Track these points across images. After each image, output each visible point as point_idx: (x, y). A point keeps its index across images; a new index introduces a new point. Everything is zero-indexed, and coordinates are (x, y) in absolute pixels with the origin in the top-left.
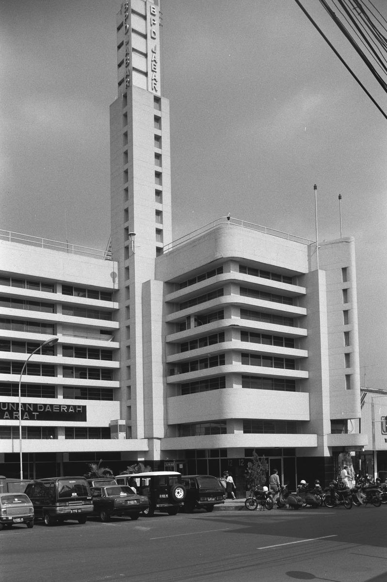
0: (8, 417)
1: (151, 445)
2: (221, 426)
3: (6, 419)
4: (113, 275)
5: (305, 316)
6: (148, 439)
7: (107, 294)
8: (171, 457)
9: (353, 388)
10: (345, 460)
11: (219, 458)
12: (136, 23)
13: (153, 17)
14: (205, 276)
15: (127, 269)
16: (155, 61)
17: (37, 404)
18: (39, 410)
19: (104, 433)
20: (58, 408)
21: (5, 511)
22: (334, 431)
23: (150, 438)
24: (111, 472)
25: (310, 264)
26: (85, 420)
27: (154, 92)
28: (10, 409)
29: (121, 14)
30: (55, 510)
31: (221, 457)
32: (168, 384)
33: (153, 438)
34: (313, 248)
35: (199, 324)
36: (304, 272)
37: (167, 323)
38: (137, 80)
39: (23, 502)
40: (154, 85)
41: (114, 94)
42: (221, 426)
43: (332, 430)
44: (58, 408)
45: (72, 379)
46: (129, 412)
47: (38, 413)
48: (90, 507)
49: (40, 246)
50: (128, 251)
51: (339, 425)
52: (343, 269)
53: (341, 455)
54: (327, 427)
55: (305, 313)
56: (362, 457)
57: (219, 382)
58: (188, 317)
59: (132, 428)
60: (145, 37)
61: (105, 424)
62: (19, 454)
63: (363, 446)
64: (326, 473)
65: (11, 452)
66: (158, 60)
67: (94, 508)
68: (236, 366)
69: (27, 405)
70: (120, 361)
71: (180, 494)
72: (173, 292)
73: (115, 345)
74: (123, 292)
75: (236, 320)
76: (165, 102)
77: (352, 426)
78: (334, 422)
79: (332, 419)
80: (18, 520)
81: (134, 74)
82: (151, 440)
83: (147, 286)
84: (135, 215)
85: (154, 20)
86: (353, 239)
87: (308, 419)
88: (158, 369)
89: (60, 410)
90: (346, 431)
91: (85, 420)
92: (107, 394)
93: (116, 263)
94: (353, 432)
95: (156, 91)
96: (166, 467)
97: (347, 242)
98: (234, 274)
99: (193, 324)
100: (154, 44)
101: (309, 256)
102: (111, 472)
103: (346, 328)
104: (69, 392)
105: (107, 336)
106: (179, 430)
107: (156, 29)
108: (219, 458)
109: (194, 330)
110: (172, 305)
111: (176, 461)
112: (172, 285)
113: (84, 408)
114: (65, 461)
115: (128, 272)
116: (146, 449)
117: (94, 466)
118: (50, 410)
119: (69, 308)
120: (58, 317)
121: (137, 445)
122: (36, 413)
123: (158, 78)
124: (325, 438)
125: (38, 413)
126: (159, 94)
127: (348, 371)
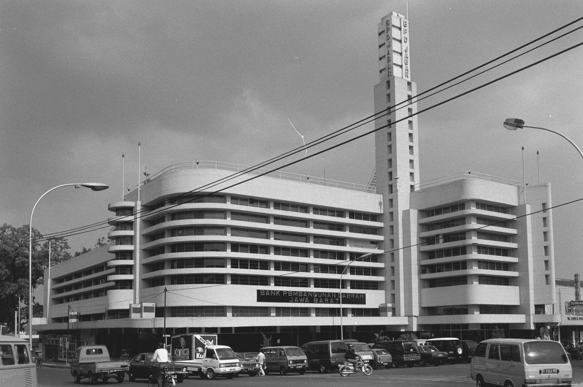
0: (322, 301)
1: (411, 321)
2: (465, 310)
3: (332, 303)
4: (380, 204)
5: (516, 234)
6: (408, 316)
7: (374, 217)
8: (425, 331)
9: (550, 284)
10: (544, 332)
12: (395, 33)
13: (405, 28)
15: (391, 200)
16: (407, 57)
17: (283, 291)
19: (374, 312)
21: (380, 359)
22: (537, 312)
23: (410, 316)
24: (388, 338)
25: (519, 200)
26: (364, 303)
27: (406, 78)
29: (382, 24)
30: (403, 359)
32: (421, 279)
33: (412, 316)
34: (521, 189)
35: (445, 241)
36: (515, 205)
37: (420, 238)
38: (397, 72)
39: (387, 354)
40: (406, 74)
41: (377, 79)
42: (465, 310)
43: (535, 312)
46: (394, 298)
48: (419, 357)
49: (335, 186)
50: (392, 189)
51: (540, 308)
52: (543, 204)
53: (542, 328)
54: (532, 310)
55: (516, 233)
56: (555, 330)
57: (463, 280)
58: (438, 235)
59: (396, 309)
60: (400, 41)
61: (376, 306)
62: (341, 326)
63: (558, 323)
65: (332, 325)
66: (409, 56)
67: (421, 357)
68: (475, 270)
69: (323, 294)
70: (385, 263)
71: (460, 352)
72: (423, 218)
73: (381, 252)
74: (388, 216)
75: (475, 240)
76: (414, 85)
77: (548, 309)
78: (537, 306)
79: (536, 304)
80: (385, 364)
81: (394, 67)
82: (410, 318)
83: (406, 213)
84: (398, 163)
85: (406, 30)
86: (550, 184)
87: (519, 304)
88: (415, 269)
89: (293, 295)
90: (544, 313)
91: (364, 303)
92: (374, 286)
93: (382, 195)
94: (548, 313)
95: (408, 77)
96: (422, 336)
97: (546, 186)
98: (474, 210)
99: (441, 241)
100: (406, 45)
101: (519, 194)
102: (388, 338)
103: (545, 244)
104: (355, 284)
105: (375, 245)
106: (428, 310)
107: (407, 35)
109: (441, 245)
110: (424, 227)
111: (430, 332)
112: (425, 212)
113: (364, 295)
114: (354, 331)
115: (392, 202)
116: (407, 323)
117: (377, 335)
118: (269, 294)
119: (354, 228)
120: (347, 234)
121: (400, 320)
123: (409, 69)
124: (532, 317)
126: (409, 80)
127: (547, 272)
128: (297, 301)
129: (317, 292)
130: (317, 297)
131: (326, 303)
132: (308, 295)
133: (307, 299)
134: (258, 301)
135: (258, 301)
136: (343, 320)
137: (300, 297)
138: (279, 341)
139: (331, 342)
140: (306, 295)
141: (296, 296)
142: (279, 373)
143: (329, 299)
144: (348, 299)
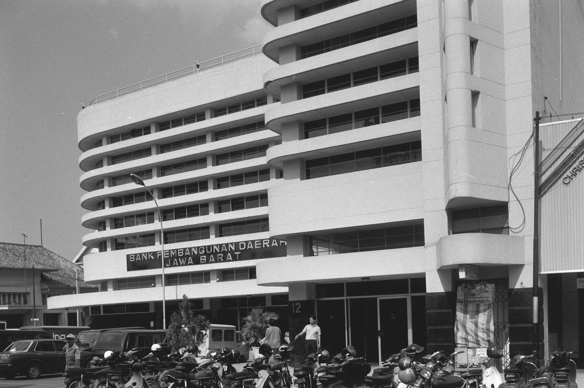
11: (344, 298)
14: (254, 102)
18: (241, 249)
20: (260, 244)
28: (214, 252)
31: (347, 296)
44: (260, 244)
45: (198, 217)
47: (240, 253)
62: (162, 302)
64: (428, 311)
65: (174, 298)
72: (157, 132)
108: (344, 298)
118: (252, 247)
122: (237, 253)
125: (240, 253)
128: (177, 264)
129: (205, 247)
130: (205, 254)
131: (220, 261)
132: (227, 249)
133: (190, 258)
134: (128, 270)
135: (128, 270)
136: (175, 297)
137: (180, 257)
138: (152, 324)
139: (380, 297)
140: (189, 254)
141: (174, 257)
142: (536, 299)
143: (225, 253)
144: (154, 261)
